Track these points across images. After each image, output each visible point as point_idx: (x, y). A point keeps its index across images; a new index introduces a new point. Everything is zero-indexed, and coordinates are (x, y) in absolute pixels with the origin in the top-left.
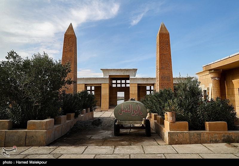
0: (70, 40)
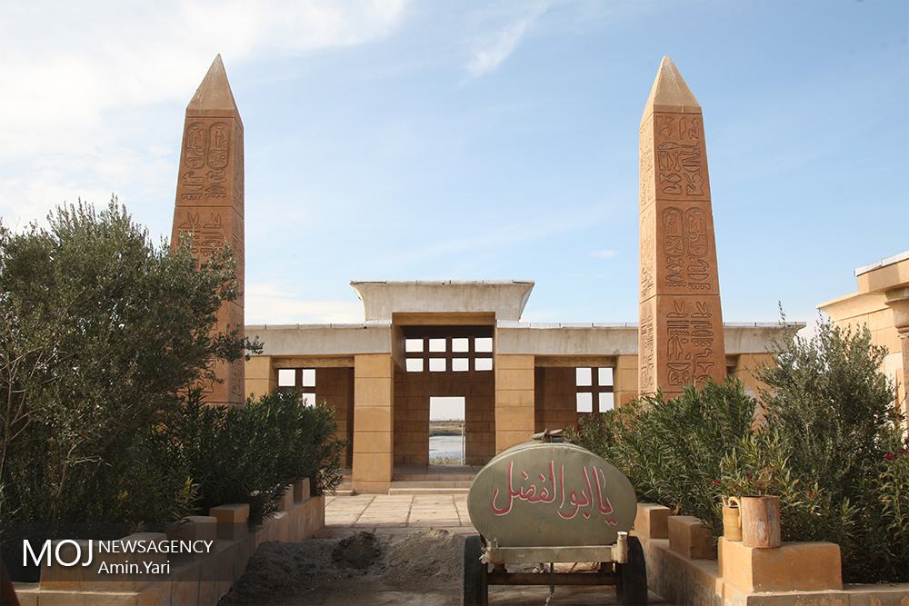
0: (213, 138)
